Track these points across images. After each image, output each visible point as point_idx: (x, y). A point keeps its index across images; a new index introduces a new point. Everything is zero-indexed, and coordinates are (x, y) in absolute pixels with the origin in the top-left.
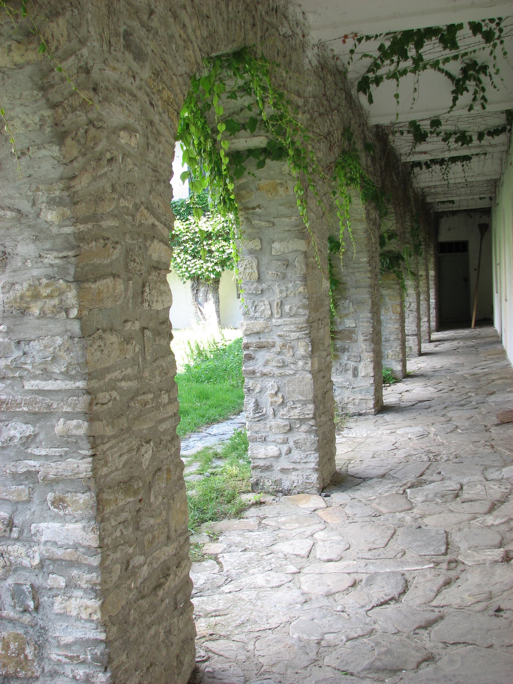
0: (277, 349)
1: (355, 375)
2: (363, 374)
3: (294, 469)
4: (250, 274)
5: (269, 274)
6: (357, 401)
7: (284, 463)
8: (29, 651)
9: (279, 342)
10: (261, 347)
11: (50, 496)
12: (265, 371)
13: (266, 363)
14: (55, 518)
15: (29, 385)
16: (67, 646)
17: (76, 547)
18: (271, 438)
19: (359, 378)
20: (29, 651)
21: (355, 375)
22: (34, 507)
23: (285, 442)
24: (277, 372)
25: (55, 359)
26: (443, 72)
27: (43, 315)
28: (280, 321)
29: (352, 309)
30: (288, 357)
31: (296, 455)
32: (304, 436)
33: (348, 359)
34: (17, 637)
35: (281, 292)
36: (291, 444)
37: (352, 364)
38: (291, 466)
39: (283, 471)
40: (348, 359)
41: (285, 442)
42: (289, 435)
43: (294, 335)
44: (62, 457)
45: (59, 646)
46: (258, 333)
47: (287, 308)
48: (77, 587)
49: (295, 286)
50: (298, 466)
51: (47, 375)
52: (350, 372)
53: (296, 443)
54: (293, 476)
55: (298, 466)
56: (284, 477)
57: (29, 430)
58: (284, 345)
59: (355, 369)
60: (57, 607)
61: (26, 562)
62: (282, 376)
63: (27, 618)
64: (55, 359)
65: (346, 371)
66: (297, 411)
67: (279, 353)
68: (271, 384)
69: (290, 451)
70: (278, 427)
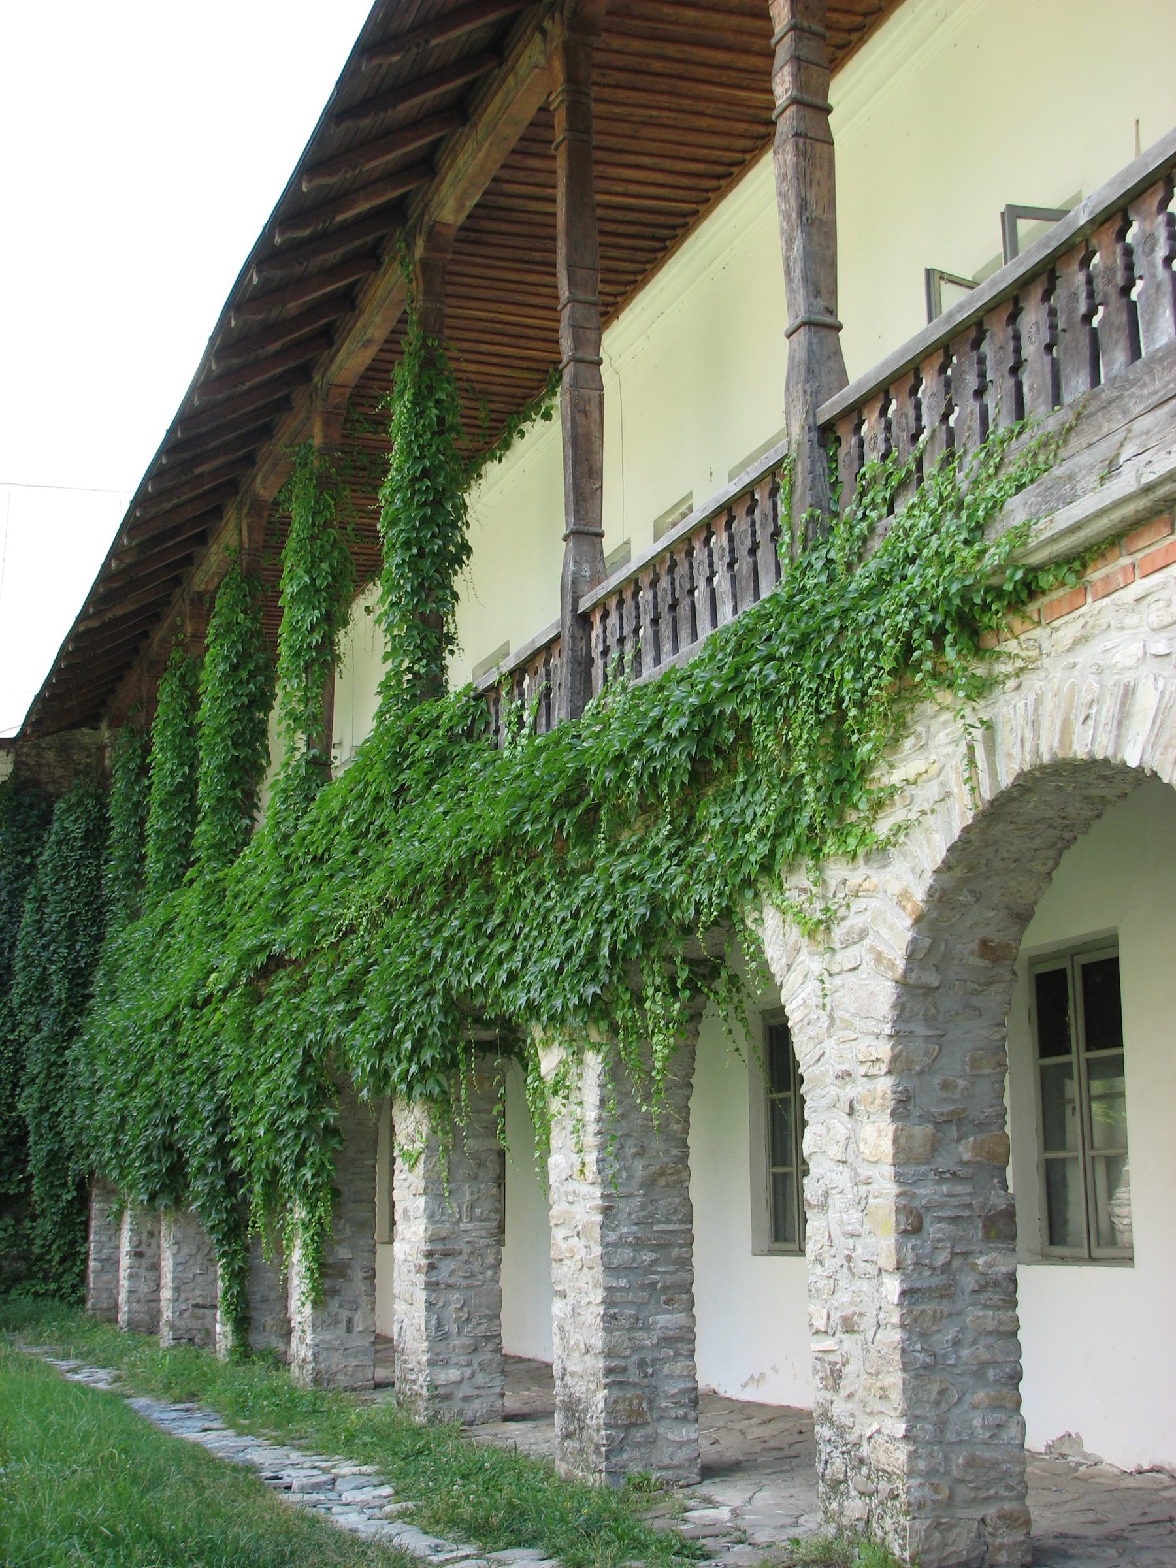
0: (465, 1257)
1: (349, 1330)
2: (360, 1328)
3: (478, 1396)
4: (439, 1173)
5: (461, 1172)
6: (350, 1369)
7: (466, 1390)
8: (645, 1405)
9: (466, 1250)
10: (447, 1254)
11: (663, 1298)
12: (450, 1282)
13: (452, 1273)
14: (666, 1312)
15: (660, 1227)
16: (673, 1396)
17: (681, 1328)
18: (454, 1360)
19: (354, 1335)
20: (645, 1405)
21: (349, 1330)
22: (651, 1306)
23: (469, 1364)
24: (463, 1283)
25: (675, 1211)
26: (1047, 1145)
27: (668, 1185)
28: (470, 1226)
29: (348, 1232)
30: (476, 1266)
31: (480, 1379)
32: (489, 1356)
33: (341, 1306)
34: (638, 1396)
35: (472, 1193)
36: (475, 1366)
37: (344, 1314)
38: (474, 1393)
39: (467, 1399)
40: (341, 1306)
41: (469, 1364)
42: (473, 1356)
43: (483, 1242)
44: (674, 1272)
45: (667, 1397)
46: (443, 1239)
47: (478, 1211)
48: (681, 1355)
49: (487, 1188)
50: (482, 1392)
51: (669, 1222)
52: (343, 1325)
53: (480, 1364)
54: (477, 1404)
55: (482, 1392)
56: (465, 1406)
57: (654, 1256)
58: (472, 1253)
59: (350, 1321)
60: (666, 1370)
61: (648, 1343)
62: (469, 1287)
63: (646, 1381)
64: (675, 1211)
65: (337, 1322)
66: (483, 1327)
67: (466, 1262)
68: (455, 1297)
69: (473, 1375)
70: (463, 1346)
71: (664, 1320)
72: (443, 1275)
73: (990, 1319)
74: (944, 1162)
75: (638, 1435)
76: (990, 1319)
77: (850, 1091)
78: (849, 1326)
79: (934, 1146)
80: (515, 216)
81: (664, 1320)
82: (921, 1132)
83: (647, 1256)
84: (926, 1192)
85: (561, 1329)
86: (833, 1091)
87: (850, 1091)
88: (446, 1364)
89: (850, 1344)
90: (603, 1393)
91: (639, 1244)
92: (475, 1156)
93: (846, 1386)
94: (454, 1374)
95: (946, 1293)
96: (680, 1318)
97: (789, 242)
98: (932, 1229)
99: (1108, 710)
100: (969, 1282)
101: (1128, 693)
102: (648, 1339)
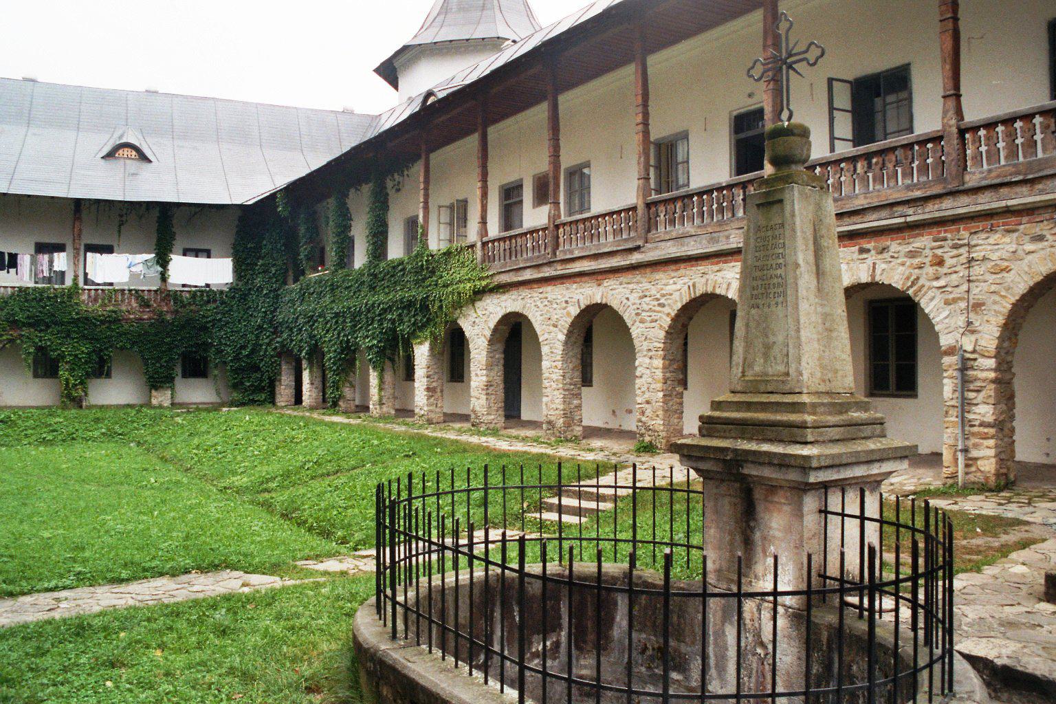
7: (496, 421)
31: (499, 418)
68: (493, 397)
71: (576, 402)
72: (489, 391)
73: (678, 400)
74: (671, 369)
75: (570, 429)
76: (678, 400)
77: (650, 354)
78: (648, 402)
79: (670, 365)
80: (834, 433)
81: (576, 402)
82: (667, 362)
83: (572, 387)
84: (668, 375)
85: (546, 404)
86: (645, 353)
87: (650, 354)
88: (491, 414)
89: (647, 406)
90: (561, 420)
91: (571, 384)
92: (498, 359)
93: (647, 414)
94: (493, 417)
95: (670, 396)
96: (579, 401)
97: (640, 157)
98: (669, 382)
99: (725, 286)
100: (674, 393)
101: (729, 284)
102: (572, 406)
